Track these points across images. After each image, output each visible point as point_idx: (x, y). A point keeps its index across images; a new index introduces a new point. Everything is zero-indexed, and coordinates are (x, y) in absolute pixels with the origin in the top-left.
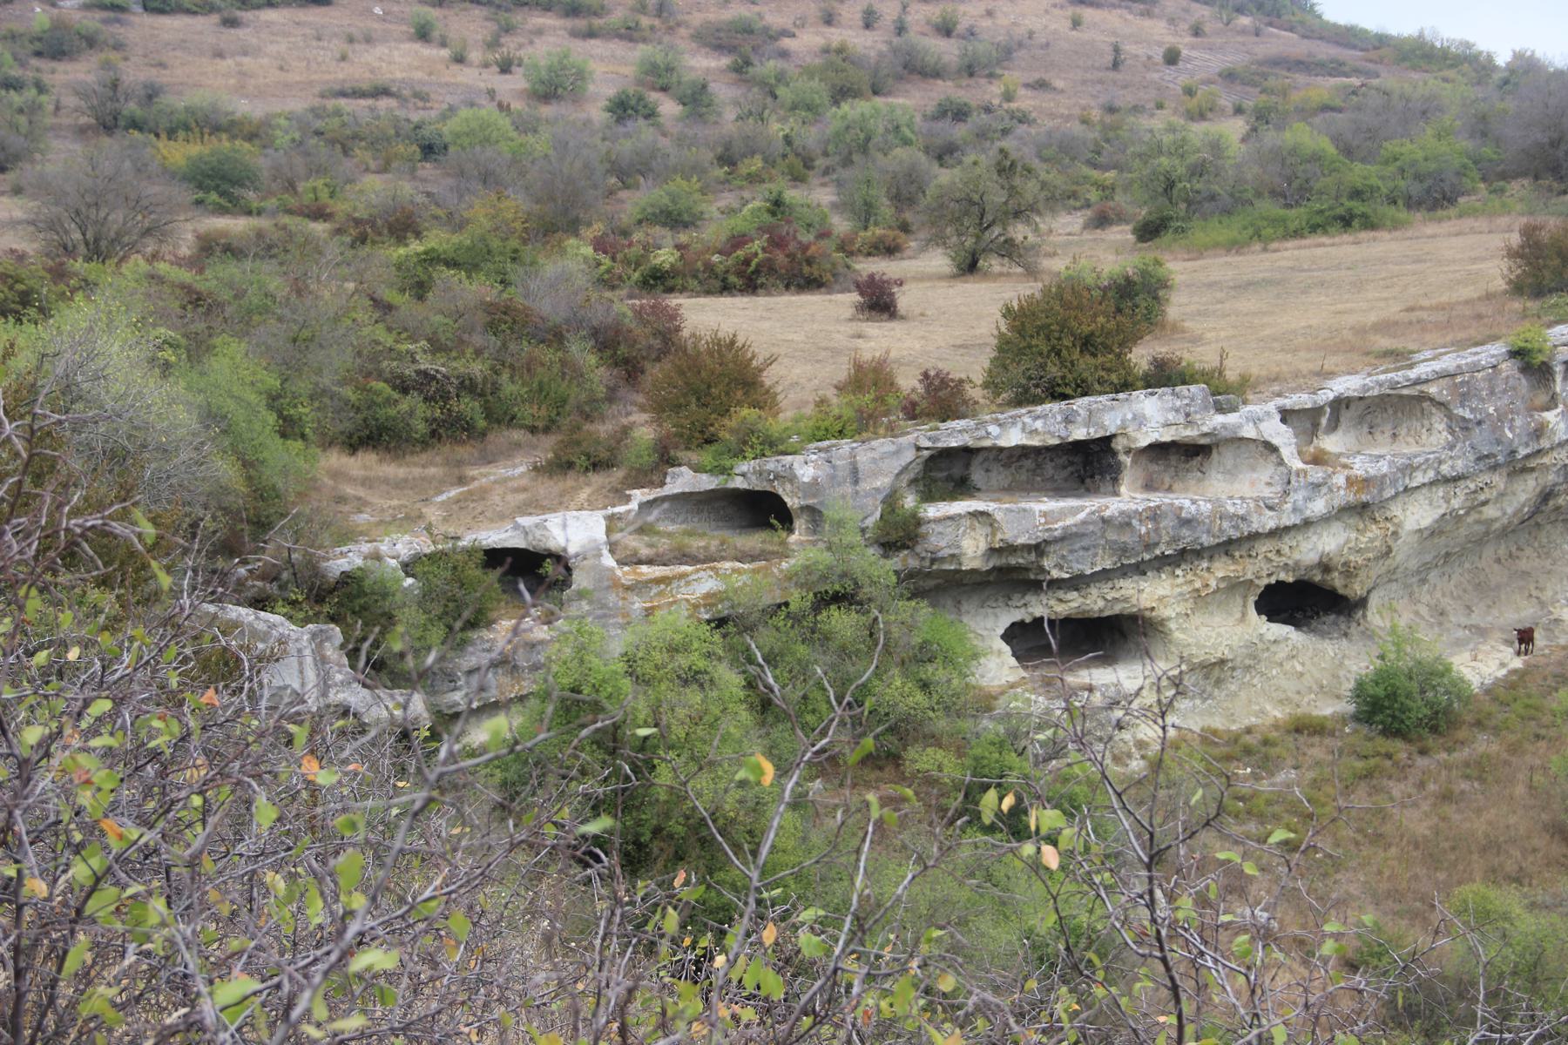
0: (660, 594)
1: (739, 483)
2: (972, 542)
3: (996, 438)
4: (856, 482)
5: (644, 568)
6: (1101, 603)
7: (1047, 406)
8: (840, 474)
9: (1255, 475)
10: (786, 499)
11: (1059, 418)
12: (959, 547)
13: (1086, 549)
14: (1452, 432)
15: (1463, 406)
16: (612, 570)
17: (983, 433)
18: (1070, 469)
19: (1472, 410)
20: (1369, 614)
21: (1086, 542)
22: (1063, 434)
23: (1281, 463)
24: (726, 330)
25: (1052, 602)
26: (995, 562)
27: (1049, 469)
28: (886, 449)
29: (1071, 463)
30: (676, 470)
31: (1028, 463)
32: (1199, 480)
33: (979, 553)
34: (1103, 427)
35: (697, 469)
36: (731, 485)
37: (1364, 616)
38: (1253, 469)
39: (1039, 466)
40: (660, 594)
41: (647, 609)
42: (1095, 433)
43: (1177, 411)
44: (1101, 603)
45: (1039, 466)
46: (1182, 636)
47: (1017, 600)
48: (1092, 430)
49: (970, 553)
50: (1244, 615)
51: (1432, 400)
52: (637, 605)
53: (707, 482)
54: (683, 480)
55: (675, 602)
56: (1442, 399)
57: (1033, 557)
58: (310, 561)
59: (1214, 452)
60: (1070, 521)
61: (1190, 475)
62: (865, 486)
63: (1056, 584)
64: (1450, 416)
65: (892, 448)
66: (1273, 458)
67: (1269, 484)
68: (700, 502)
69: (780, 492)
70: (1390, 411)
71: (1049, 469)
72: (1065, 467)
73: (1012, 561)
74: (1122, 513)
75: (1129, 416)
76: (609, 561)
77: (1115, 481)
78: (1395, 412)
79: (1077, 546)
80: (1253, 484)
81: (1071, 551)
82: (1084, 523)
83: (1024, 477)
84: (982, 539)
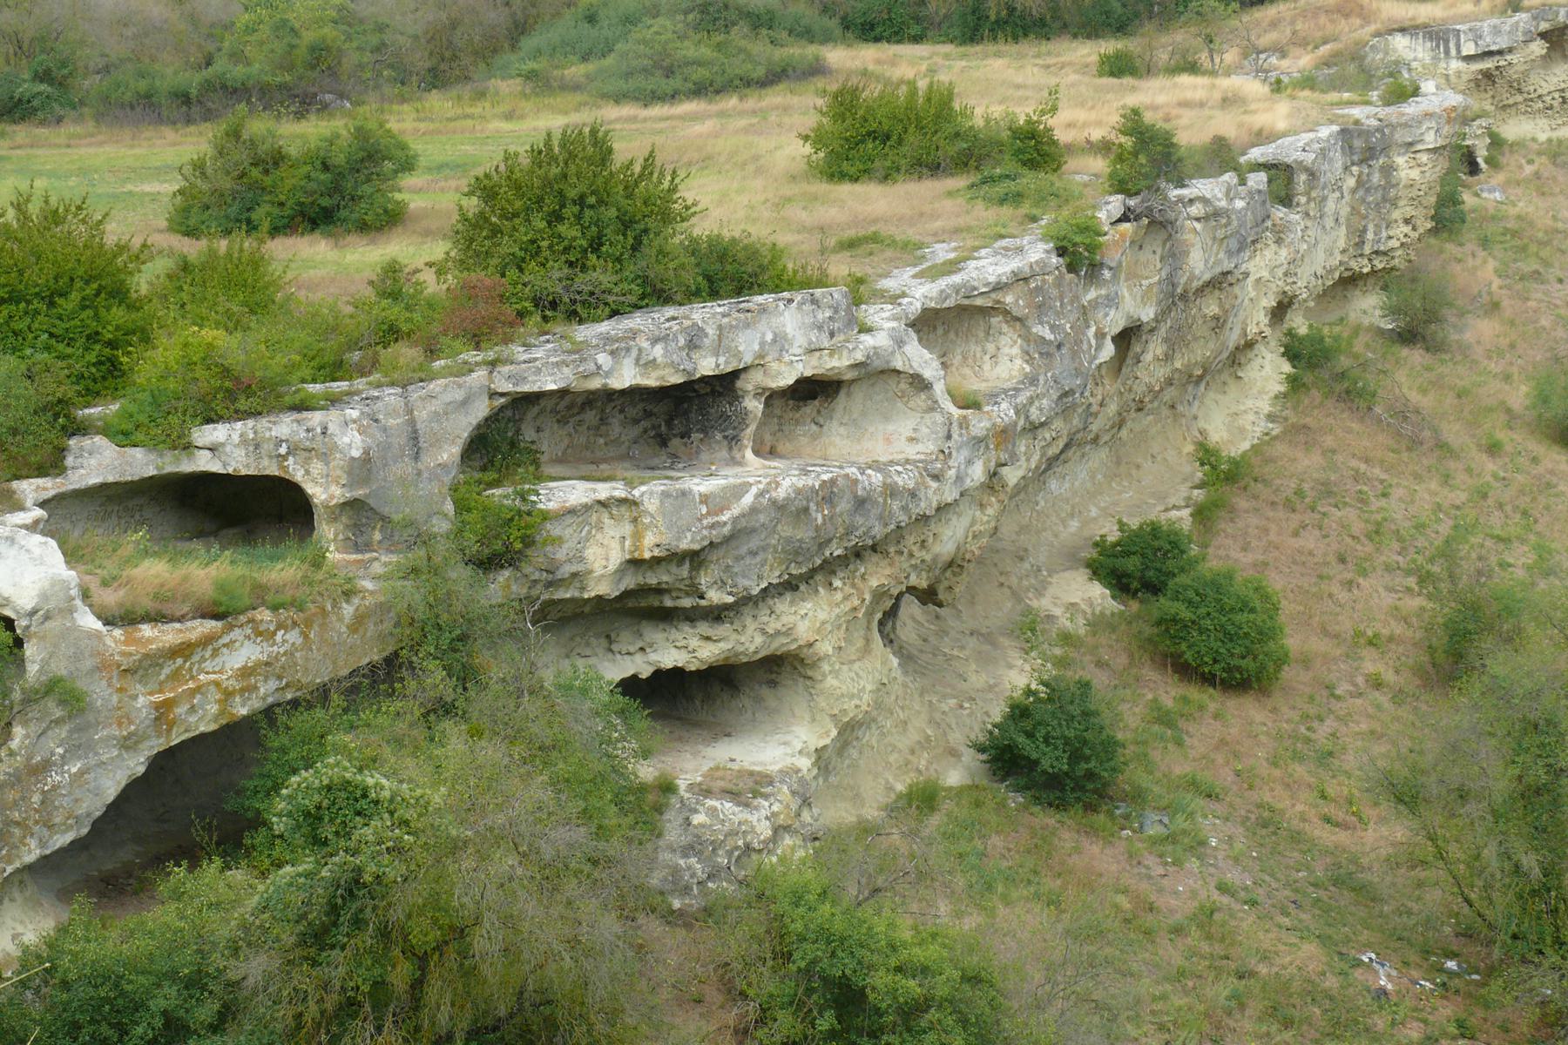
0: (176, 676)
1: (204, 463)
2: (599, 551)
3: (608, 374)
4: (417, 457)
5: (147, 630)
6: (759, 640)
7: (636, 321)
8: (395, 441)
9: (890, 428)
10: (310, 489)
11: (682, 342)
12: (582, 559)
13: (753, 554)
14: (1030, 361)
15: (1041, 323)
16: (98, 635)
17: (592, 367)
18: (644, 424)
19: (1053, 328)
20: (898, 623)
21: (754, 543)
22: (689, 367)
23: (934, 407)
24: (67, 189)
25: (694, 643)
26: (629, 582)
27: (616, 427)
28: (448, 397)
29: (648, 414)
30: (87, 442)
31: (591, 416)
32: (814, 437)
33: (612, 567)
34: (738, 355)
35: (123, 436)
36: (187, 467)
37: (894, 628)
38: (887, 418)
39: (603, 421)
40: (176, 676)
41: (158, 706)
42: (725, 365)
43: (820, 328)
44: (759, 640)
45: (603, 421)
46: (835, 683)
47: (626, 641)
48: (722, 360)
49: (599, 572)
50: (868, 641)
51: (1006, 313)
52: (141, 699)
53: (141, 463)
54: (98, 462)
55: (198, 690)
56: (1019, 315)
57: (685, 571)
58: (1101, 794)
59: (843, 393)
60: (736, 511)
61: (800, 430)
62: (428, 461)
63: (717, 614)
64: (1027, 337)
65: (459, 395)
66: (921, 400)
67: (911, 440)
68: (110, 498)
69: (298, 476)
70: (940, 331)
71: (616, 427)
72: (636, 421)
73: (652, 580)
74: (798, 492)
75: (769, 337)
76: (88, 621)
77: (733, 440)
78: (946, 332)
79: (744, 550)
80: (888, 441)
81: (738, 558)
82: (754, 510)
83: (583, 440)
84: (615, 545)
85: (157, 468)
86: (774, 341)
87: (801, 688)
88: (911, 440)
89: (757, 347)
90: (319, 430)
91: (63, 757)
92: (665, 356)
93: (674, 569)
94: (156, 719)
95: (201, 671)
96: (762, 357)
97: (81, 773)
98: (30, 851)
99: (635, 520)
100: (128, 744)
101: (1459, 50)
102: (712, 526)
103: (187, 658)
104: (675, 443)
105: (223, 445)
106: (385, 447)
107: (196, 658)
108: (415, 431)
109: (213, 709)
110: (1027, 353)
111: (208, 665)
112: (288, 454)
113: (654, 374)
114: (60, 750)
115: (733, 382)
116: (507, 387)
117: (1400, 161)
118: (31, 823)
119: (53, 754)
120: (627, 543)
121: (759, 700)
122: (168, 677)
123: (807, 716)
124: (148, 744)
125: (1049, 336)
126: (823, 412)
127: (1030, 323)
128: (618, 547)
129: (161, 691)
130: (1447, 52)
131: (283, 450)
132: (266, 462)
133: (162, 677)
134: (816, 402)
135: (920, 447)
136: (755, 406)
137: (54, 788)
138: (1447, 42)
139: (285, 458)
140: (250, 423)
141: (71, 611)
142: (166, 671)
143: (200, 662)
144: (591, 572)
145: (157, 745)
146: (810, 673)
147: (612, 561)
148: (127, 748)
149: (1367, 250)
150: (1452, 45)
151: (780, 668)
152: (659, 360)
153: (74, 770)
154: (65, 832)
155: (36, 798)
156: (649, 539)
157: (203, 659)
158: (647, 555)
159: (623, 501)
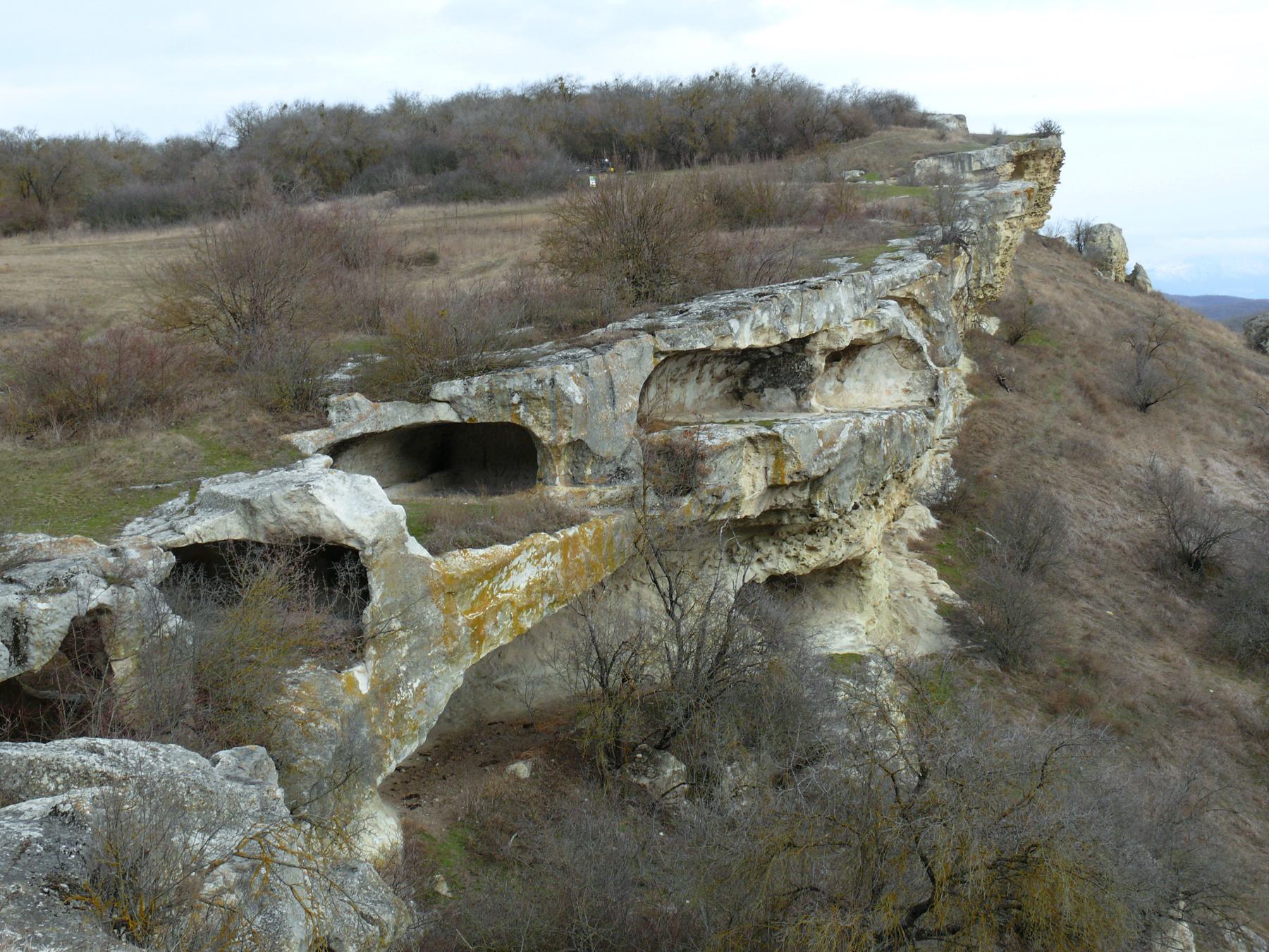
4: (613, 404)
10: (538, 432)
19: (943, 313)
53: (399, 415)
57: (805, 495)
69: (530, 422)
75: (832, 308)
79: (843, 476)
85: (634, 393)
86: (835, 311)
87: (853, 587)
88: (907, 391)
89: (824, 316)
90: (547, 382)
91: (406, 674)
92: (769, 322)
93: (797, 493)
94: (473, 635)
95: (500, 591)
96: (828, 324)
97: (422, 687)
98: (390, 763)
99: (776, 454)
100: (451, 658)
101: (970, 168)
102: (828, 457)
103: (491, 579)
104: (750, 396)
105: (460, 397)
106: (594, 396)
107: (496, 580)
108: (612, 383)
109: (509, 624)
110: (927, 332)
111: (504, 586)
112: (520, 403)
113: (763, 337)
114: (404, 668)
115: (804, 345)
116: (665, 347)
117: (1000, 224)
118: (389, 736)
119: (399, 672)
120: (770, 472)
121: (817, 597)
122: (477, 597)
123: (857, 608)
124: (465, 658)
125: (942, 320)
126: (846, 371)
127: (930, 309)
128: (763, 476)
129: (472, 611)
130: (963, 169)
131: (515, 399)
132: (500, 411)
133: (474, 598)
134: (840, 363)
135: (913, 397)
136: (819, 362)
137: (404, 703)
138: (962, 162)
139: (517, 406)
140: (487, 377)
141: (401, 542)
142: (476, 592)
143: (499, 583)
144: (743, 496)
145: (469, 659)
146: (863, 574)
147: (758, 487)
148: (452, 662)
149: (982, 283)
150: (966, 164)
151: (849, 571)
152: (766, 325)
153: (416, 685)
154: (412, 741)
155: (391, 713)
156: (789, 467)
157: (501, 581)
158: (787, 481)
159: (766, 438)
